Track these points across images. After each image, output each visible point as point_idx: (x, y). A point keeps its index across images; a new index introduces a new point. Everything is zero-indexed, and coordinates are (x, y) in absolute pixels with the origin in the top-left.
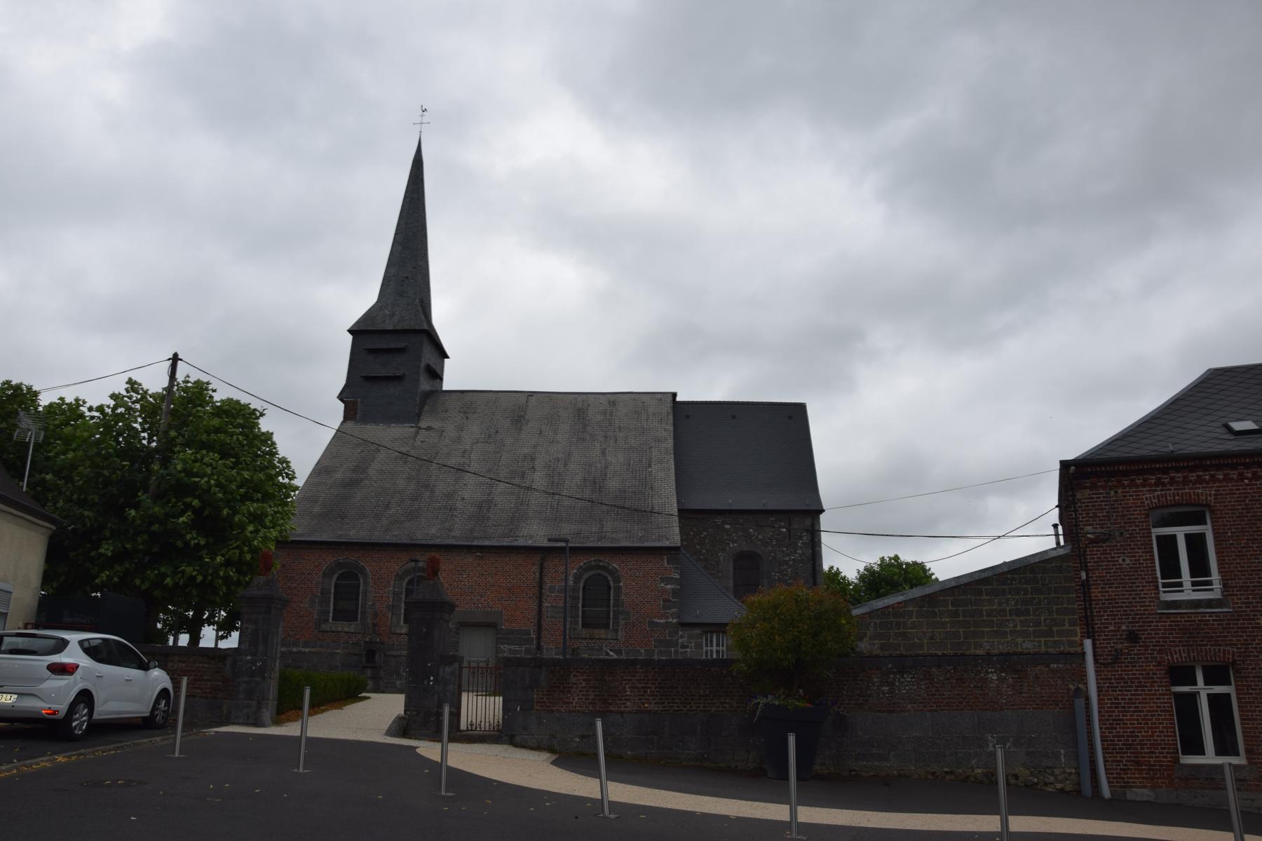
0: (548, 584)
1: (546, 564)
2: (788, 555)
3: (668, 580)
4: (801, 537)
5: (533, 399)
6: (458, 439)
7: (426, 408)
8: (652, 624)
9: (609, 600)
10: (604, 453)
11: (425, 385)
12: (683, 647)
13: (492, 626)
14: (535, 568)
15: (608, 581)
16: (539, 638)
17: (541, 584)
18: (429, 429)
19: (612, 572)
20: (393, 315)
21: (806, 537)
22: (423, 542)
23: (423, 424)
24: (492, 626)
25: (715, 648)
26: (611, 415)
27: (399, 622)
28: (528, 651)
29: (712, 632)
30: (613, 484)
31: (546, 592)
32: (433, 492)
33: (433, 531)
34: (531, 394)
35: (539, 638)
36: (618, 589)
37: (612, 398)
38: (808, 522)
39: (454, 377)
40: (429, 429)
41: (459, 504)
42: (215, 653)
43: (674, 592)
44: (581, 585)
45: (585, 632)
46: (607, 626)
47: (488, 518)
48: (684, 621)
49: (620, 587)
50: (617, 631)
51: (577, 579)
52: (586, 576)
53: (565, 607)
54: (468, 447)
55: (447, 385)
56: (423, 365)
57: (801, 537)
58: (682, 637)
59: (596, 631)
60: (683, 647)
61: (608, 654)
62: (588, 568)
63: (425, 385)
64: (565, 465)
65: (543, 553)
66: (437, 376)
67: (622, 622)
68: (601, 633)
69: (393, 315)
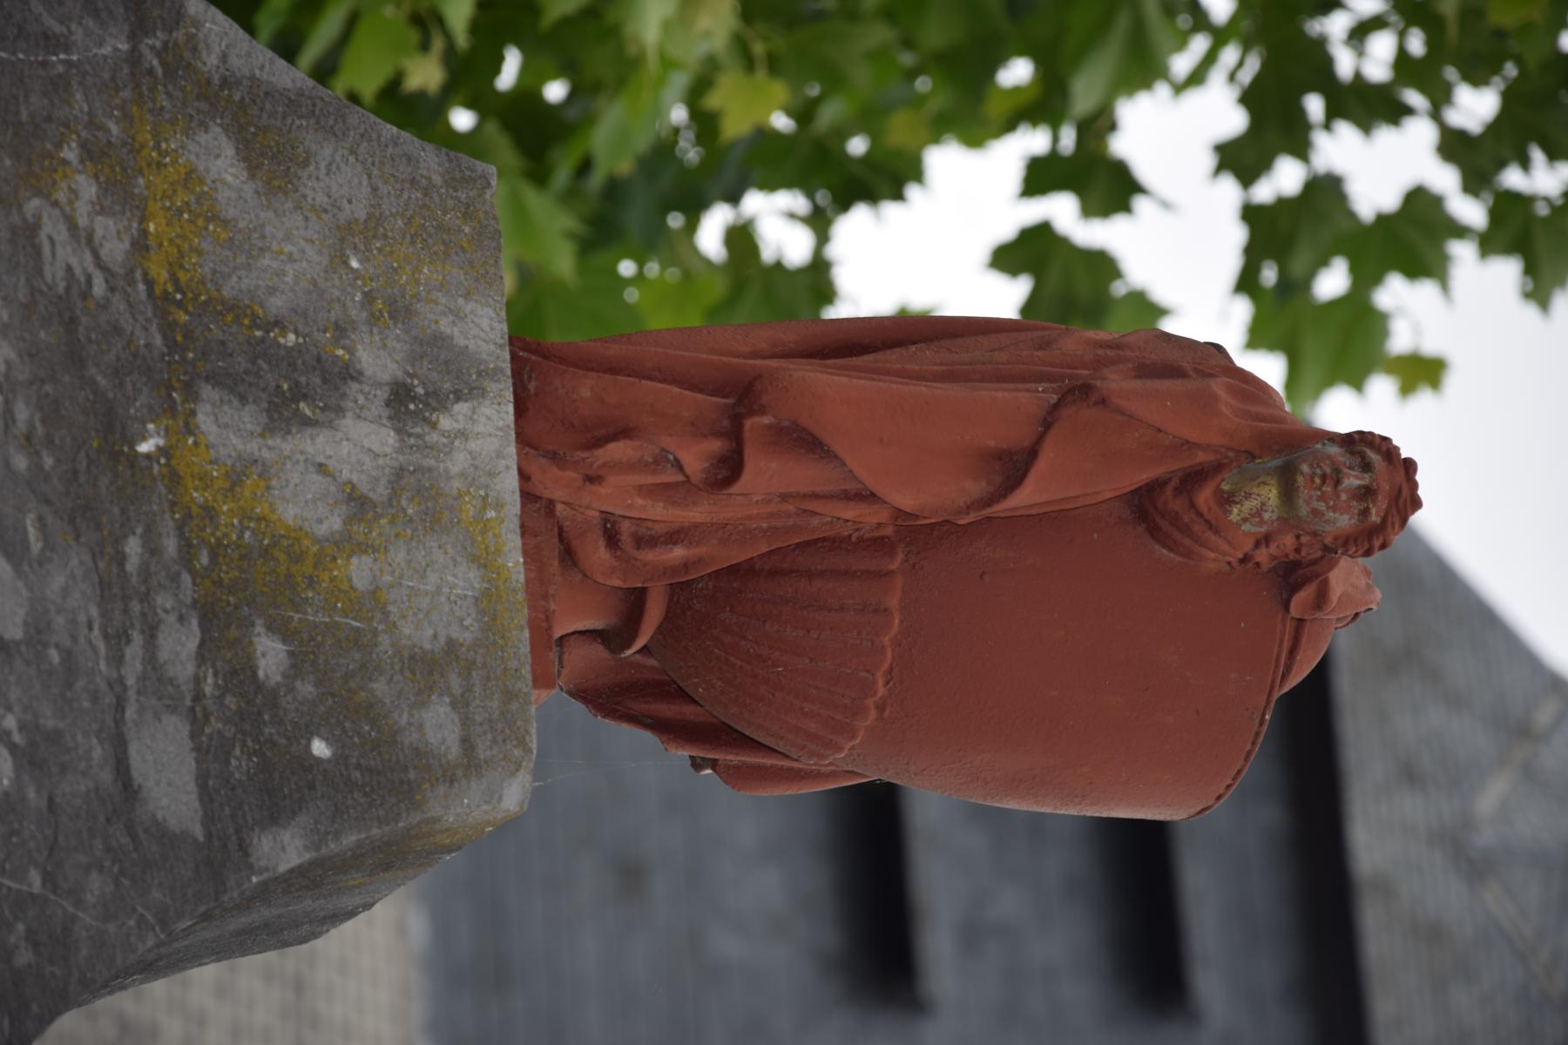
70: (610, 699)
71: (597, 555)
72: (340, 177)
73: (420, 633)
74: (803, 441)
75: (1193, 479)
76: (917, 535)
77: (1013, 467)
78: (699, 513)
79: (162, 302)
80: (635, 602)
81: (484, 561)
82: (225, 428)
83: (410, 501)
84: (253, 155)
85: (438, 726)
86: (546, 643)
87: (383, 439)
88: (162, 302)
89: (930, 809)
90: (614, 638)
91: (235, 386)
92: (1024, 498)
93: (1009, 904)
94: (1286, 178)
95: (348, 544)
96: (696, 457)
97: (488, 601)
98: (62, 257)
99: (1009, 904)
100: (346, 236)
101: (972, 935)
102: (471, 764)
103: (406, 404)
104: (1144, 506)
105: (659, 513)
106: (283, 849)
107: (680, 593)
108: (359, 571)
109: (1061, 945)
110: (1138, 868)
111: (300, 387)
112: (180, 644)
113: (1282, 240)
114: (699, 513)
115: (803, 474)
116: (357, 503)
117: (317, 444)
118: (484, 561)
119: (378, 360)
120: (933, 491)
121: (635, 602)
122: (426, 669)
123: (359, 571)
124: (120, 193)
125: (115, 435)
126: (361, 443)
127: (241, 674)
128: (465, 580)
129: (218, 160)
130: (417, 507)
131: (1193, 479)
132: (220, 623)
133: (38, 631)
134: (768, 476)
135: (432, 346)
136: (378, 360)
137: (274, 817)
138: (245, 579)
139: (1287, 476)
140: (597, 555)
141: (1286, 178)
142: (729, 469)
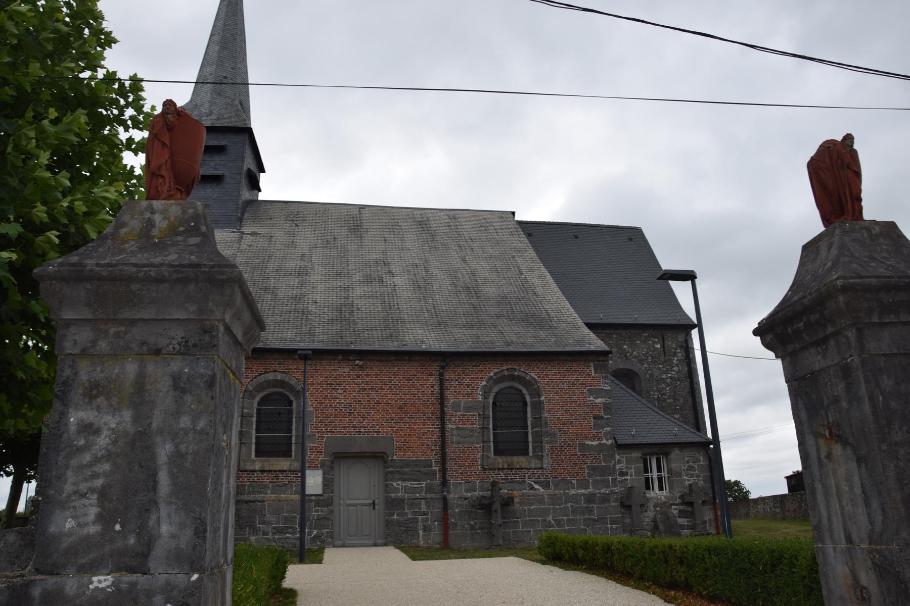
0: (451, 400)
1: (446, 375)
2: (666, 372)
3: (598, 393)
4: (675, 354)
5: (366, 211)
6: (293, 244)
7: (246, 215)
8: (583, 447)
9: (525, 419)
10: (464, 260)
11: (246, 195)
12: (622, 474)
13: (378, 457)
14: (432, 380)
15: (523, 395)
16: (444, 471)
17: (442, 399)
18: (253, 234)
19: (529, 384)
20: (211, 113)
21: (680, 354)
22: (281, 346)
23: (246, 230)
24: (378, 457)
25: (655, 474)
26: (456, 227)
27: (249, 455)
28: (429, 489)
29: (652, 454)
30: (489, 290)
31: (449, 410)
32: (274, 294)
33: (289, 335)
34: (362, 207)
35: (444, 471)
36: (538, 407)
37: (451, 213)
38: (681, 338)
39: (271, 189)
40: (253, 234)
41: (312, 308)
42: (114, 148)
43: (607, 407)
44: (491, 400)
45: (501, 461)
46: (525, 452)
47: (355, 323)
48: (621, 442)
49: (540, 403)
50: (541, 458)
51: (486, 392)
52: (496, 389)
53: (484, 428)
54: (306, 252)
55: (262, 196)
56: (245, 168)
57: (675, 354)
58: (619, 462)
59: (515, 459)
60: (622, 474)
61: (532, 488)
62: (500, 379)
63: (246, 195)
64: (427, 271)
65: (445, 359)
66: (255, 186)
67: (547, 446)
68: (519, 461)
69: (211, 113)
70: (188, 193)
71: (172, 193)
72: (126, 218)
73: (180, 212)
74: (160, 168)
75: (167, 124)
76: (171, 157)
77: (164, 144)
78: (167, 181)
79: (140, 238)
80: (178, 189)
81: (172, 205)
82: (155, 232)
83: (164, 212)
84: (123, 227)
85: (191, 211)
86: (181, 199)
87: (157, 215)
88: (140, 238)
89: (202, 172)
90: (181, 192)
91: (150, 231)
92: (168, 143)
93: (212, 164)
94: (129, 122)
95: (169, 220)
96: (161, 180)
97: (176, 205)
98: (134, 248)
99: (212, 164)
100: (133, 217)
101: (216, 169)
102: (195, 208)
103: (153, 212)
104: (170, 130)
105: (167, 185)
106: (204, 228)
107: (177, 184)
108: (172, 219)
109: (217, 159)
110: (209, 150)
111: (150, 224)
112: (180, 238)
113: (137, 125)
114: (167, 181)
115: (163, 168)
116: (164, 218)
117: (157, 222)
118: (172, 205)
119: (148, 215)
120: (166, 154)
121: (178, 189)
122: (184, 212)
123: (172, 219)
124: (127, 242)
125: (155, 244)
126: (157, 218)
127: (183, 232)
128: (174, 207)
129: (124, 231)
130: (166, 212)
131: (167, 124)
132: (178, 234)
133: (177, 253)
134: (163, 172)
135: (146, 209)
136: (148, 215)
137: (200, 229)
138: (173, 231)
139: (167, 114)
140: (172, 193)
141: (129, 122)
142: (162, 177)
